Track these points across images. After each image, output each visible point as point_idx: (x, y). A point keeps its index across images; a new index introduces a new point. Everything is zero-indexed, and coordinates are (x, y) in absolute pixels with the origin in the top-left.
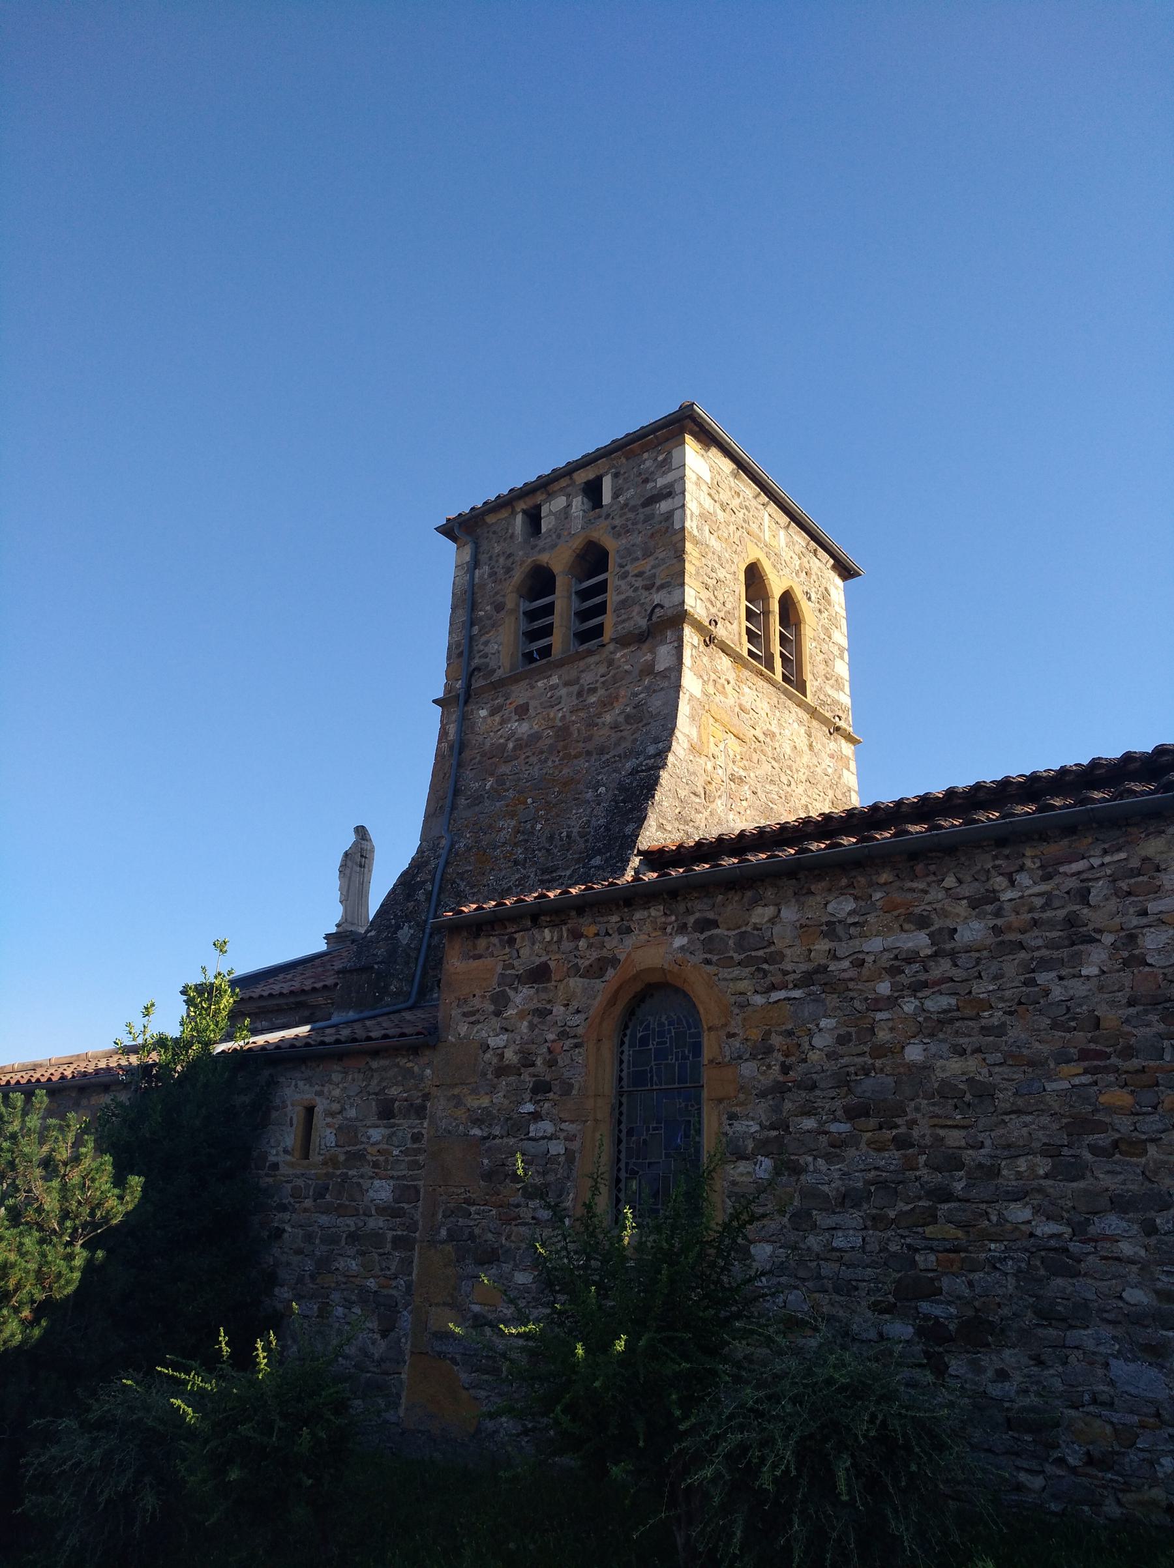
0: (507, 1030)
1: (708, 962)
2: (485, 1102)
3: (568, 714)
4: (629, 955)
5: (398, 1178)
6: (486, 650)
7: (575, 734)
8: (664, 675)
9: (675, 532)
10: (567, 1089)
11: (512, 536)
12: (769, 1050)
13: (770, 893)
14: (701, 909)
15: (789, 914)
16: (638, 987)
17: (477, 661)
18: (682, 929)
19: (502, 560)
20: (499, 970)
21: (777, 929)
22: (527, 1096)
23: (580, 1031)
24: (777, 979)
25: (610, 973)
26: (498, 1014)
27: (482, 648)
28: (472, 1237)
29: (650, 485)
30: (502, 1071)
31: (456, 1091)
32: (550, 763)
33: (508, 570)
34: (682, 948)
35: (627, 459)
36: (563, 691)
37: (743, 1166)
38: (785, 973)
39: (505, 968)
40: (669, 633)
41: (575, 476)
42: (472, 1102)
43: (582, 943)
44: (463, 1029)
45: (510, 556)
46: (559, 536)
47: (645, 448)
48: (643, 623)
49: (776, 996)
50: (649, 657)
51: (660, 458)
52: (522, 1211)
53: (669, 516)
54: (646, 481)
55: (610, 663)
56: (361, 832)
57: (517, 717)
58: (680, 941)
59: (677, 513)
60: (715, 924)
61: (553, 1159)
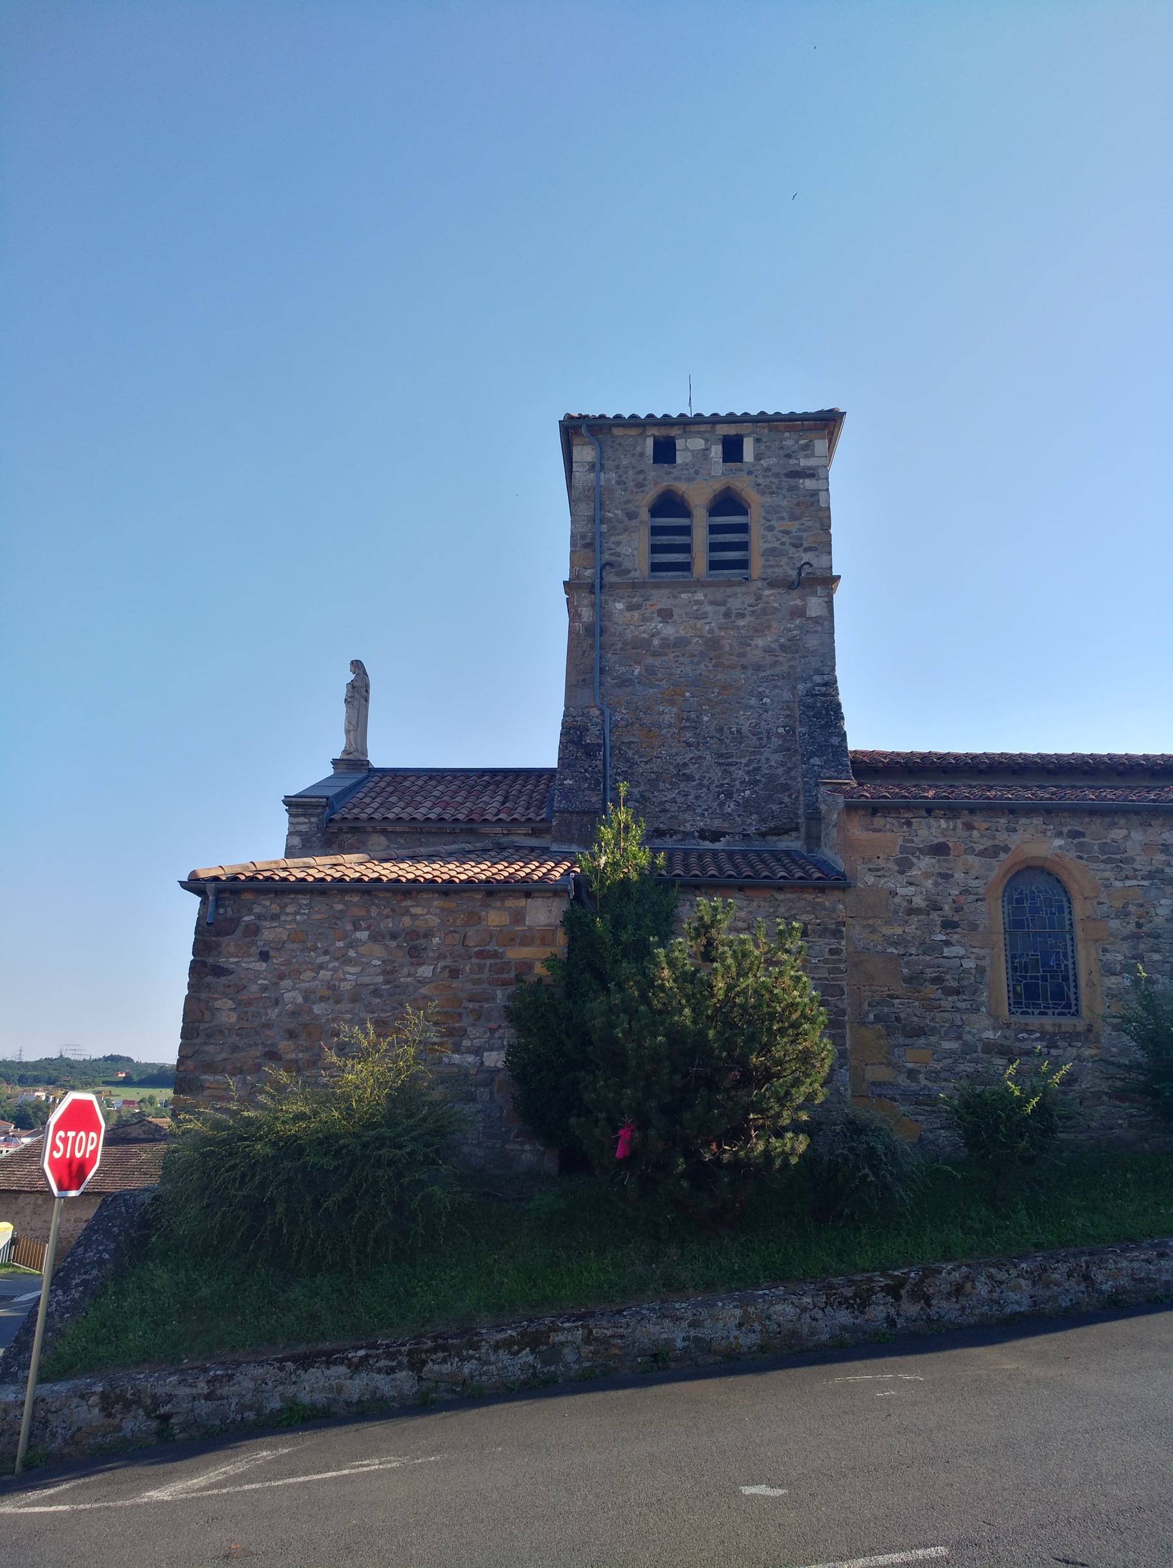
0: (911, 884)
1: (1081, 858)
2: (899, 931)
3: (716, 630)
4: (1019, 846)
5: (820, 979)
6: (618, 550)
7: (727, 648)
8: (817, 621)
9: (821, 509)
10: (973, 927)
11: (642, 455)
12: (1127, 914)
13: (1122, 822)
14: (1072, 824)
15: (1137, 835)
16: (1020, 867)
17: (607, 557)
18: (1059, 834)
19: (631, 473)
20: (900, 842)
21: (1129, 844)
22: (938, 929)
23: (981, 890)
24: (1131, 873)
25: (1003, 856)
26: (902, 872)
27: (613, 546)
28: (898, 1019)
29: (792, 461)
30: (912, 911)
31: (871, 922)
32: (702, 666)
33: (640, 485)
34: (1060, 847)
35: (770, 431)
36: (709, 608)
37: (1114, 979)
38: (1136, 870)
39: (905, 841)
40: (819, 588)
41: (718, 427)
42: (887, 931)
43: (975, 833)
44: (870, 880)
45: (641, 472)
46: (697, 472)
47: (788, 429)
48: (794, 573)
49: (1128, 883)
50: (798, 602)
51: (802, 442)
52: (943, 1003)
53: (814, 494)
54: (789, 456)
55: (759, 597)
56: (357, 666)
57: (660, 619)
58: (1058, 842)
59: (822, 495)
60: (1083, 835)
61: (967, 971)
